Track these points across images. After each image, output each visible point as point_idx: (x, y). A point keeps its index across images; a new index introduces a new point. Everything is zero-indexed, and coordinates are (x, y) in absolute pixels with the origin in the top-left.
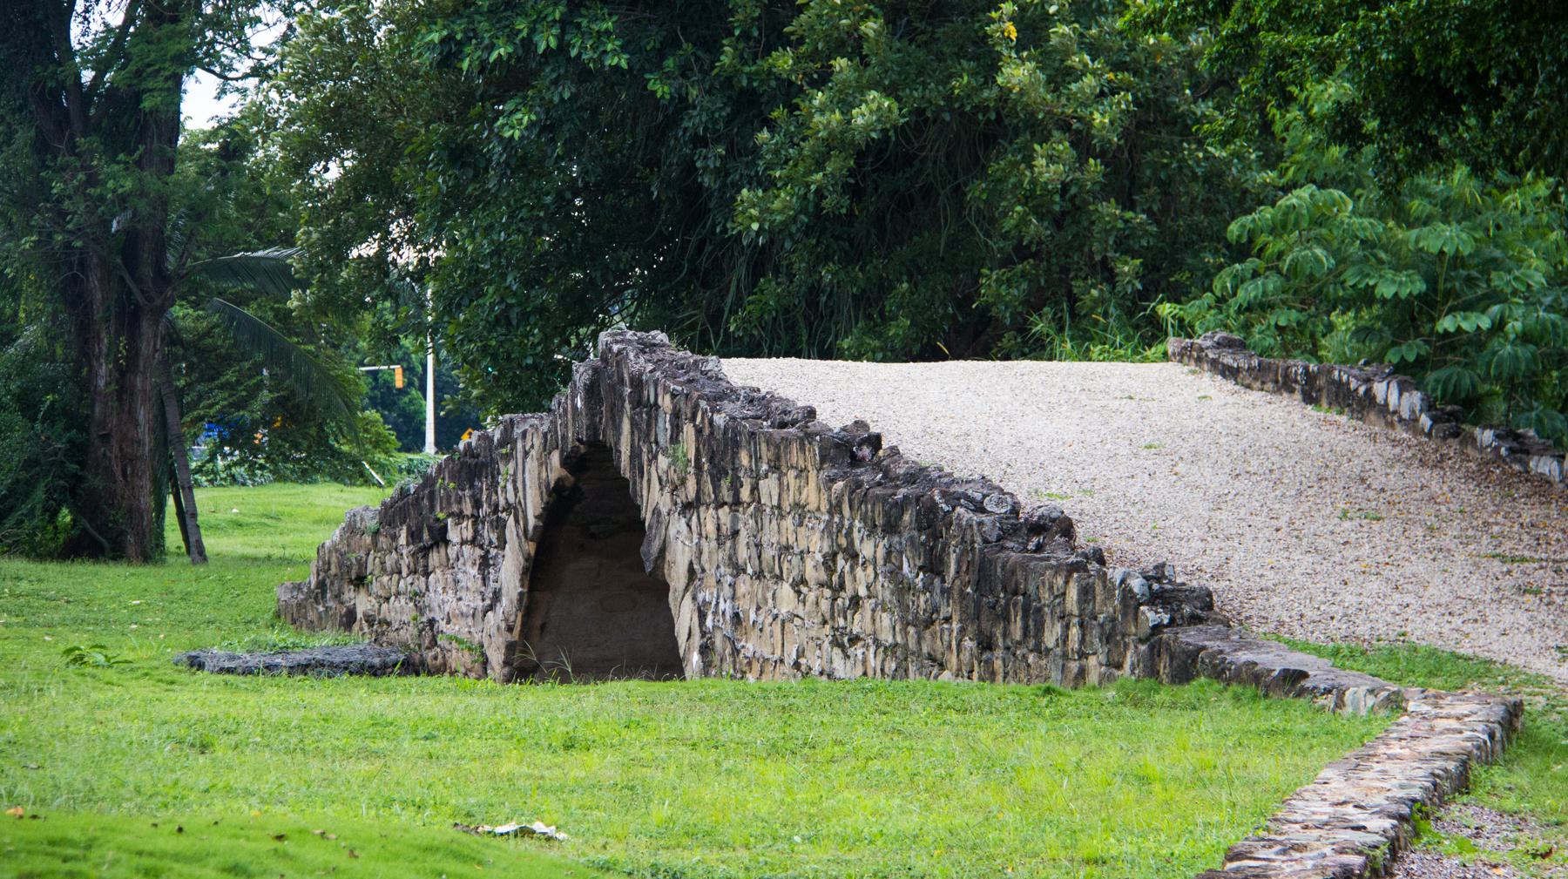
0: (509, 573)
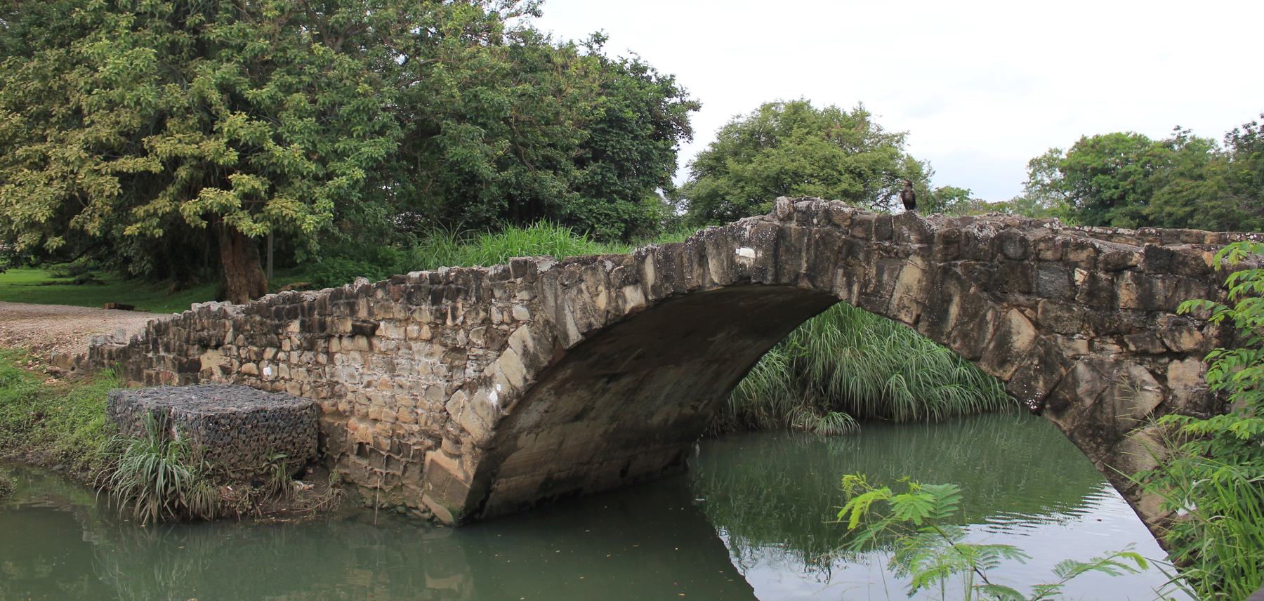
0: (509, 370)
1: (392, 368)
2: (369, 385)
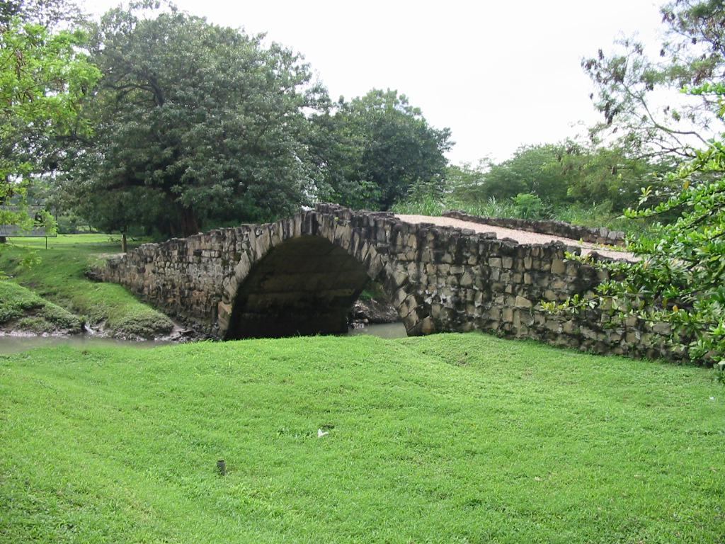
1: (206, 269)
2: (200, 276)
